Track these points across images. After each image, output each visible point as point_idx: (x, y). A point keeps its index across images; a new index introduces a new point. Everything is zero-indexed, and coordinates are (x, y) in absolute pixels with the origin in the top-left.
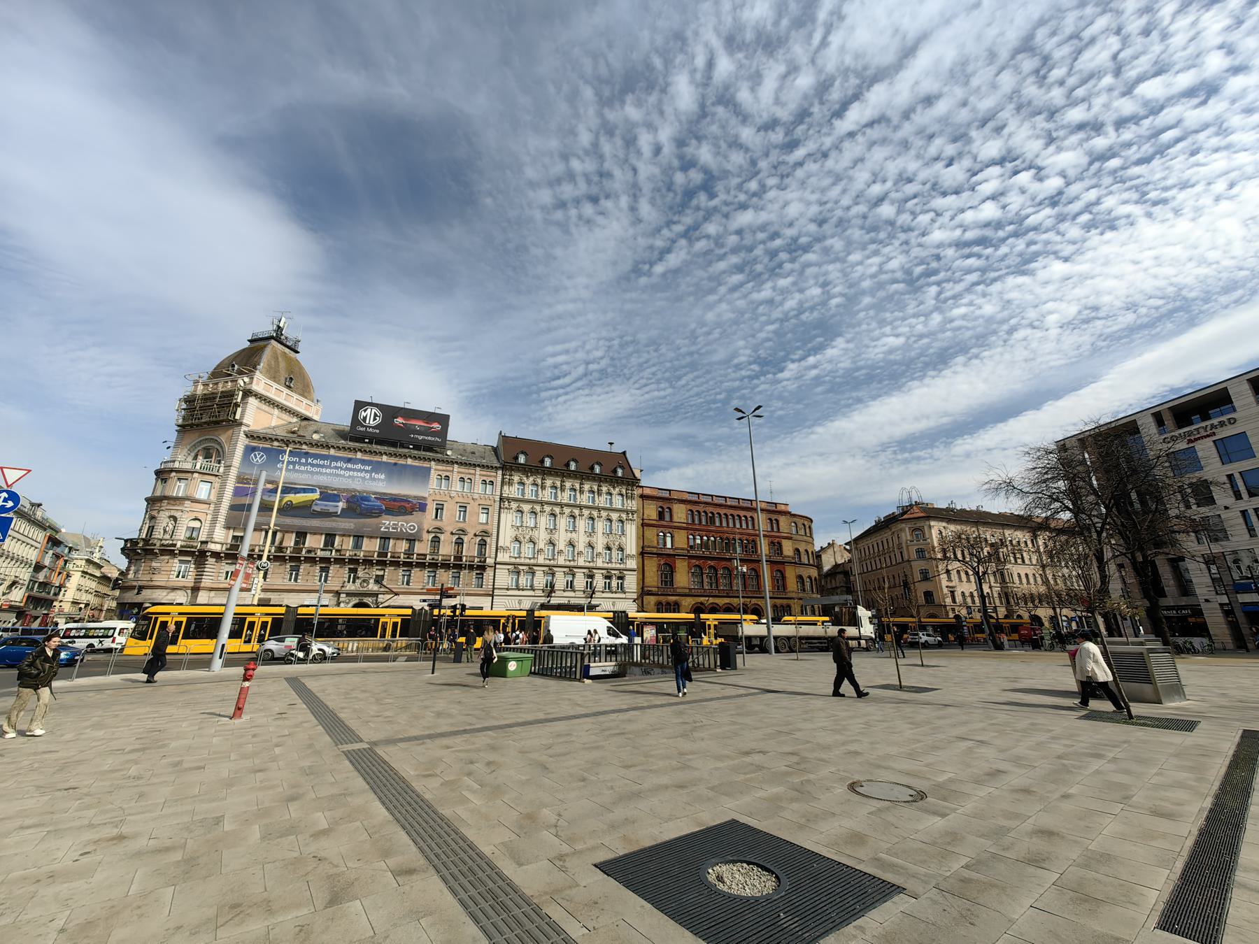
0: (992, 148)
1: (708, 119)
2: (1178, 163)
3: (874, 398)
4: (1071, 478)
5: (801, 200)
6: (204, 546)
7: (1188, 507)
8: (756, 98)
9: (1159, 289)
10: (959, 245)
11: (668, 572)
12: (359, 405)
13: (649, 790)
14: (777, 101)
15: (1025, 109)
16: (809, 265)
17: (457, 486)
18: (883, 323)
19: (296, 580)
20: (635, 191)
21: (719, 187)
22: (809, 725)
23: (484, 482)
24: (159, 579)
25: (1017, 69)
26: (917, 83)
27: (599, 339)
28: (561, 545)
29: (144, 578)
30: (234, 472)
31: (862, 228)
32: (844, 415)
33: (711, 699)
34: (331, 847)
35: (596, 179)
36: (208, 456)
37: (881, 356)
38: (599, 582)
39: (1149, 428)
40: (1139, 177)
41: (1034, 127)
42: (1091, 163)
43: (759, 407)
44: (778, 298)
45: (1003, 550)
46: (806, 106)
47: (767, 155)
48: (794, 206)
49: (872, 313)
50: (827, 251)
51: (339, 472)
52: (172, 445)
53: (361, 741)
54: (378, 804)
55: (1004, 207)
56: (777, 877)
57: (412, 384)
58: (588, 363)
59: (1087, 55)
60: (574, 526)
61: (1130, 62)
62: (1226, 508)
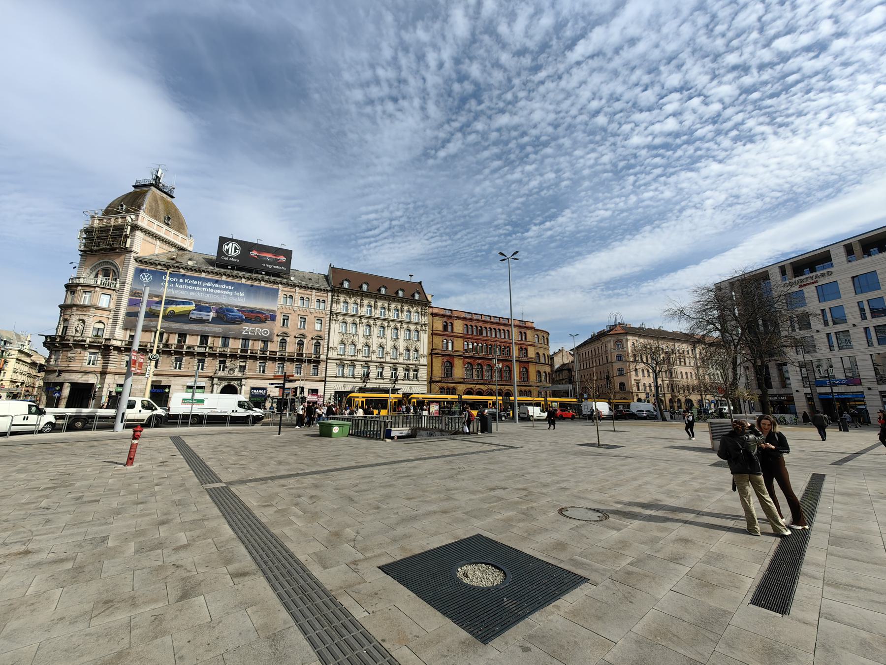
0: (674, 80)
1: (478, 45)
2: (797, 100)
3: (590, 252)
4: (722, 309)
5: (542, 109)
6: (108, 342)
7: (794, 330)
8: (511, 31)
9: (779, 185)
10: (650, 147)
11: (449, 367)
12: (223, 241)
13: (423, 515)
14: (527, 35)
15: (699, 53)
16: (547, 156)
17: (298, 303)
18: (597, 201)
19: (180, 368)
20: (424, 94)
21: (485, 96)
22: (535, 470)
23: (319, 301)
24: (74, 366)
25: (694, 23)
26: (625, 28)
27: (399, 203)
28: (374, 347)
29: (62, 364)
30: (127, 288)
31: (584, 132)
32: (569, 263)
33: (473, 453)
34: (187, 558)
35: (396, 84)
36: (106, 274)
37: (595, 223)
38: (401, 373)
39: (775, 276)
40: (770, 107)
41: (704, 66)
42: (740, 95)
43: (517, 252)
44: (526, 179)
45: (673, 357)
46: (548, 40)
47: (519, 74)
48: (538, 112)
49: (590, 193)
50: (560, 147)
51: (209, 290)
52: (77, 265)
53: (221, 481)
54: (227, 526)
55: (681, 123)
56: (504, 573)
57: (262, 226)
58: (391, 220)
59: (741, 16)
60: (384, 334)
61: (770, 23)
62: (818, 331)
